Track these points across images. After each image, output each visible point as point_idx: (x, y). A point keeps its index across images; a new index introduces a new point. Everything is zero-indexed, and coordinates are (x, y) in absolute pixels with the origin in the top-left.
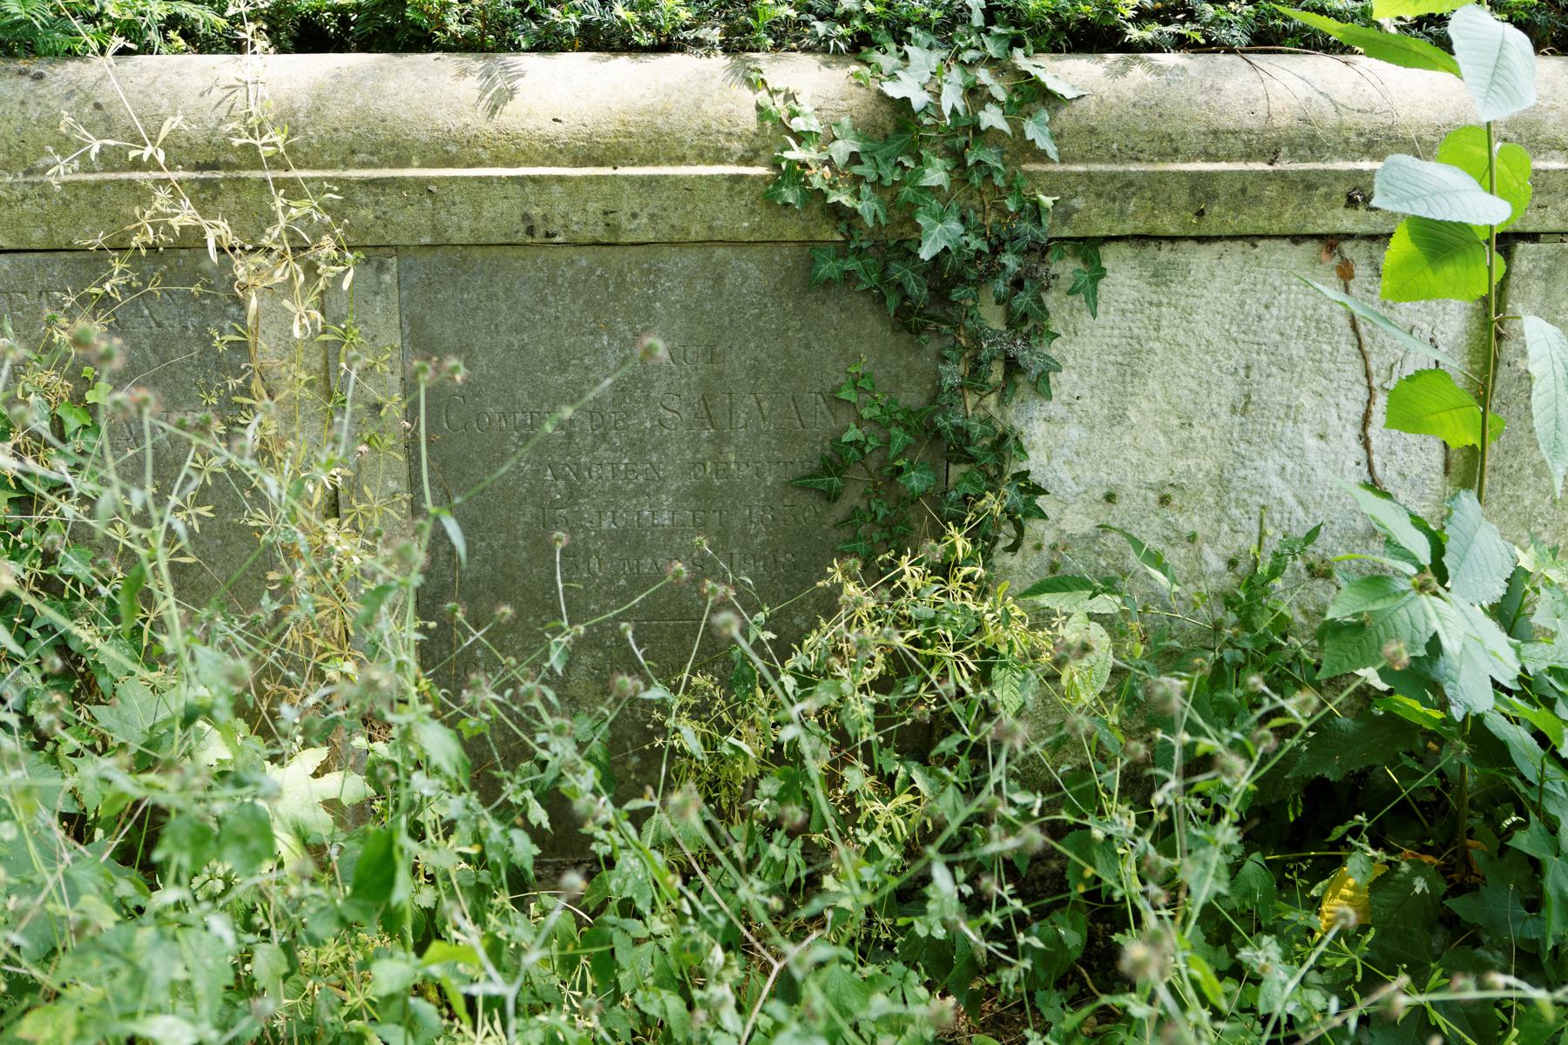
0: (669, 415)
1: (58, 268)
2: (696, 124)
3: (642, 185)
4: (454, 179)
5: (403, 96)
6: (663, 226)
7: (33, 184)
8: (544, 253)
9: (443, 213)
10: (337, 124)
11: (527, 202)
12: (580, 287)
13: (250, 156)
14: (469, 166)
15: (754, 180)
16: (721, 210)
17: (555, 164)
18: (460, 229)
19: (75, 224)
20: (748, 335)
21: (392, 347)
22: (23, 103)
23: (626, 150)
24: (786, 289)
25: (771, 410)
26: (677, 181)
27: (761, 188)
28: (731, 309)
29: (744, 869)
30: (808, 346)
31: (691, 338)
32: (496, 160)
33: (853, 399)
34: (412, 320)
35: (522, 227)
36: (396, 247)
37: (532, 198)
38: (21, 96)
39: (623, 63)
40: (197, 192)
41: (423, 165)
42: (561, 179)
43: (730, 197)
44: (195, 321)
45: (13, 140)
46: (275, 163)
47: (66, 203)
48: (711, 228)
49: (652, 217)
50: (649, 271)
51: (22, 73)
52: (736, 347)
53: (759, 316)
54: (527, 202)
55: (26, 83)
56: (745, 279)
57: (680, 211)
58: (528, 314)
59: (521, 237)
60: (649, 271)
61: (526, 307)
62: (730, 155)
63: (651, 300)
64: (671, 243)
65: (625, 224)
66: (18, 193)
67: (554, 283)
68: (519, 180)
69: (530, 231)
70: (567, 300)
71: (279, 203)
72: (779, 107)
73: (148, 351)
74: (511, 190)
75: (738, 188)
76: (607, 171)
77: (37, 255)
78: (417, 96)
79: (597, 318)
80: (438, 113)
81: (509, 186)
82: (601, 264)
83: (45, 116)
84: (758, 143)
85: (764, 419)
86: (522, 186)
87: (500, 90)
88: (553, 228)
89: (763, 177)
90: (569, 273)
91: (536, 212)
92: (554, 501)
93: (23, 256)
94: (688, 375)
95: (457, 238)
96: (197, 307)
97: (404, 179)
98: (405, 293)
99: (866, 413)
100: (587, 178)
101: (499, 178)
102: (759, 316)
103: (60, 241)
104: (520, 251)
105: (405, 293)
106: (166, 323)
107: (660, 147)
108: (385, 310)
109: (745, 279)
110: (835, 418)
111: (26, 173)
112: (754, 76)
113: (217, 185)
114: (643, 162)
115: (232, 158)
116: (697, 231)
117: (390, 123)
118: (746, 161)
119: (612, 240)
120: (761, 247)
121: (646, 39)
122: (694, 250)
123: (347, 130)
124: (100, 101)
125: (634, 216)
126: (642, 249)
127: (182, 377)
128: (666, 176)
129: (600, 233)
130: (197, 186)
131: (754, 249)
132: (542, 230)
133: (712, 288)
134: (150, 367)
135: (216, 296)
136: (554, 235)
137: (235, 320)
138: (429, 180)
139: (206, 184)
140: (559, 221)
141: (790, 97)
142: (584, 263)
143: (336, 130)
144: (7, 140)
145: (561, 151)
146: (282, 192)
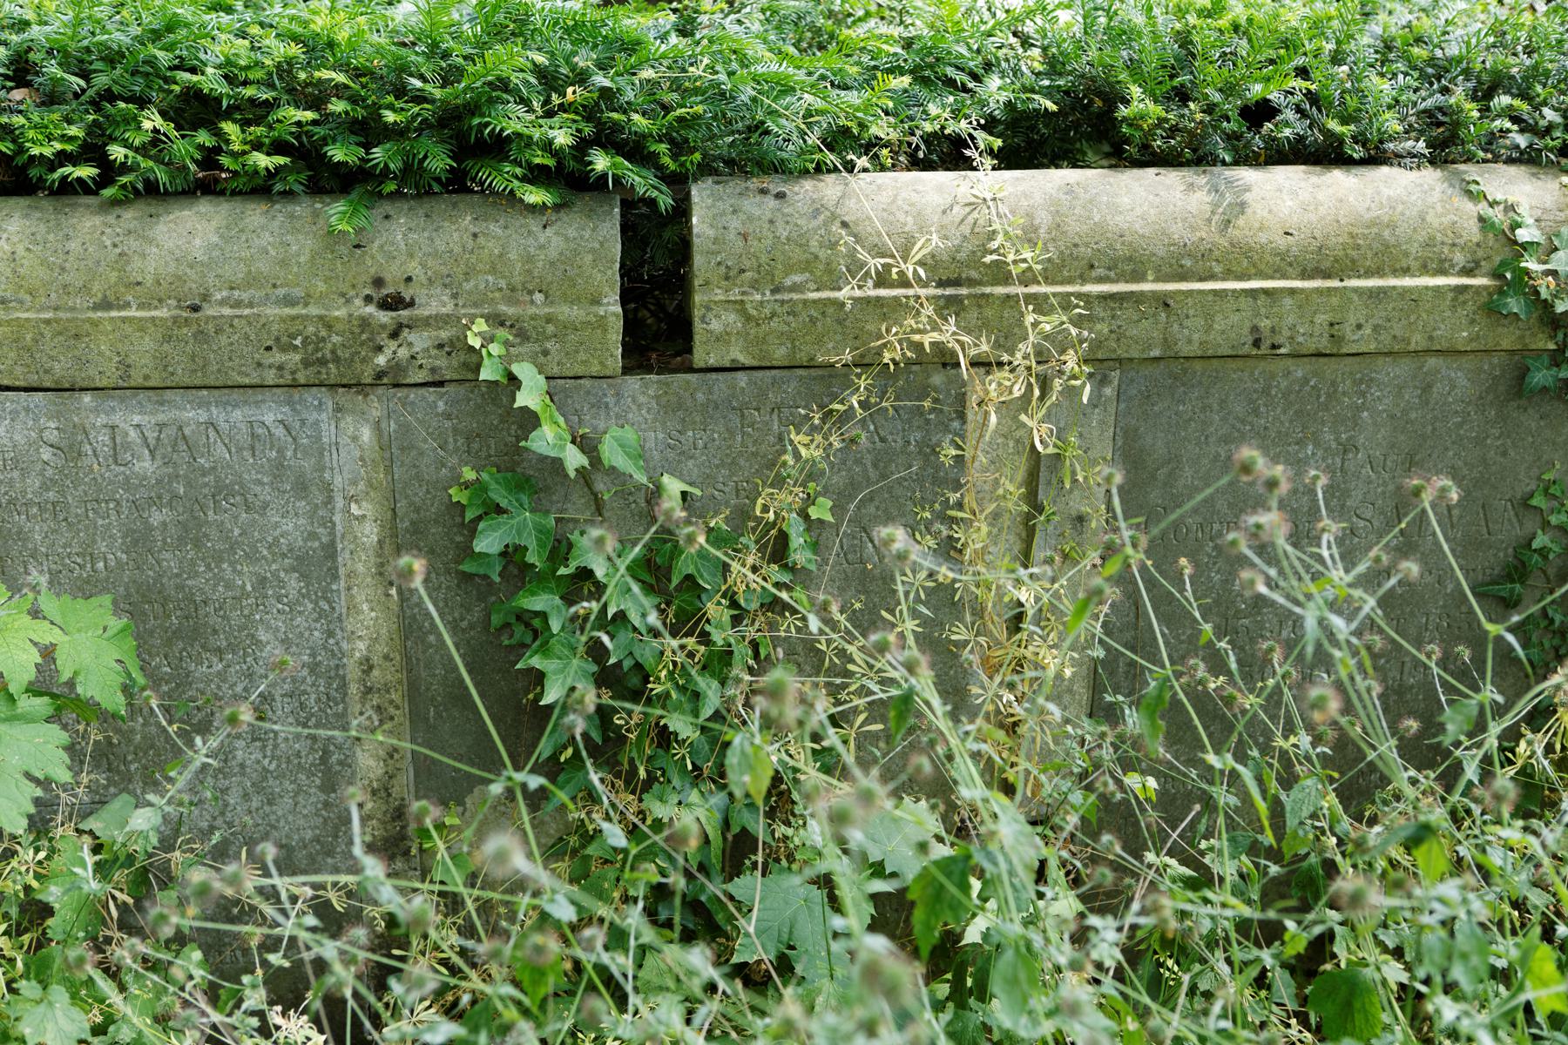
0: (1362, 524)
1: (794, 384)
2: (1422, 236)
3: (1370, 297)
4: (1190, 293)
5: (1138, 211)
6: (1385, 338)
7: (783, 302)
8: (1263, 364)
9: (1176, 326)
10: (1077, 240)
11: (1258, 315)
12: (1292, 397)
13: (1000, 274)
14: (1201, 280)
15: (1478, 290)
16: (1443, 321)
17: (1284, 277)
18: (1190, 341)
19: (819, 341)
20: (1448, 444)
21: (1104, 459)
22: (771, 222)
23: (1353, 261)
24: (1490, 397)
25: (1461, 517)
26: (1405, 291)
27: (1484, 298)
28: (1435, 418)
29: (1237, 970)
30: (1504, 454)
31: (1393, 446)
32: (1228, 274)
33: (1543, 506)
34: (1126, 433)
35: (1250, 340)
36: (1120, 360)
37: (1263, 311)
38: (769, 215)
39: (1337, 175)
40: (942, 308)
41: (1157, 280)
42: (1292, 291)
43: (1453, 308)
44: (918, 435)
45: (764, 259)
46: (1027, 278)
47: (813, 320)
48: (1431, 338)
49: (1376, 328)
50: (1361, 381)
51: (763, 192)
52: (1435, 456)
53: (1460, 425)
54: (1258, 315)
55: (771, 203)
56: (1453, 387)
57: (1404, 322)
58: (1238, 425)
59: (1248, 349)
60: (1361, 381)
61: (1237, 418)
62: (1452, 266)
63: (1360, 409)
64: (1389, 354)
65: (1350, 336)
66: (767, 311)
67: (1268, 394)
68: (1253, 293)
69: (1257, 343)
70: (1279, 410)
71: (1030, 319)
72: (1497, 215)
73: (869, 465)
74: (1244, 303)
75: (1461, 298)
76: (1335, 283)
77: (774, 372)
78: (1152, 211)
79: (1304, 427)
80: (1174, 228)
81: (1242, 299)
82: (1315, 374)
83: (794, 235)
84: (1480, 253)
85: (1452, 526)
86: (1255, 299)
87: (1230, 204)
88: (1279, 340)
89: (1485, 288)
90: (1284, 384)
91: (1265, 324)
92: (1238, 611)
93: (760, 374)
94: (1385, 484)
95: (1186, 350)
96: (921, 422)
97: (1142, 293)
98: (1122, 406)
99: (1554, 520)
100: (1317, 290)
101: (1234, 291)
102: (1460, 425)
103: (802, 357)
104: (1240, 363)
105: (1122, 406)
106: (890, 438)
107: (1387, 258)
108: (1102, 422)
109: (1453, 387)
110: (1521, 524)
111: (773, 292)
112: (1473, 187)
113: (961, 302)
114: (1369, 274)
115: (974, 274)
116: (1418, 341)
117: (1128, 238)
118: (1467, 272)
119: (1335, 351)
120: (1472, 356)
121: (1358, 152)
122: (1406, 360)
123: (1087, 245)
124: (846, 219)
125: (1359, 327)
126: (1358, 359)
127: (898, 491)
128: (1394, 288)
129: (1324, 344)
130: (942, 302)
131: (1464, 359)
132: (1268, 343)
133: (1420, 397)
134: (869, 483)
135: (941, 411)
136: (1279, 347)
137: (956, 434)
138: (1166, 294)
139: (951, 300)
140: (1286, 333)
141: (1510, 208)
142: (1300, 374)
143: (1076, 245)
144: (757, 258)
145: (1291, 265)
146: (1031, 308)
